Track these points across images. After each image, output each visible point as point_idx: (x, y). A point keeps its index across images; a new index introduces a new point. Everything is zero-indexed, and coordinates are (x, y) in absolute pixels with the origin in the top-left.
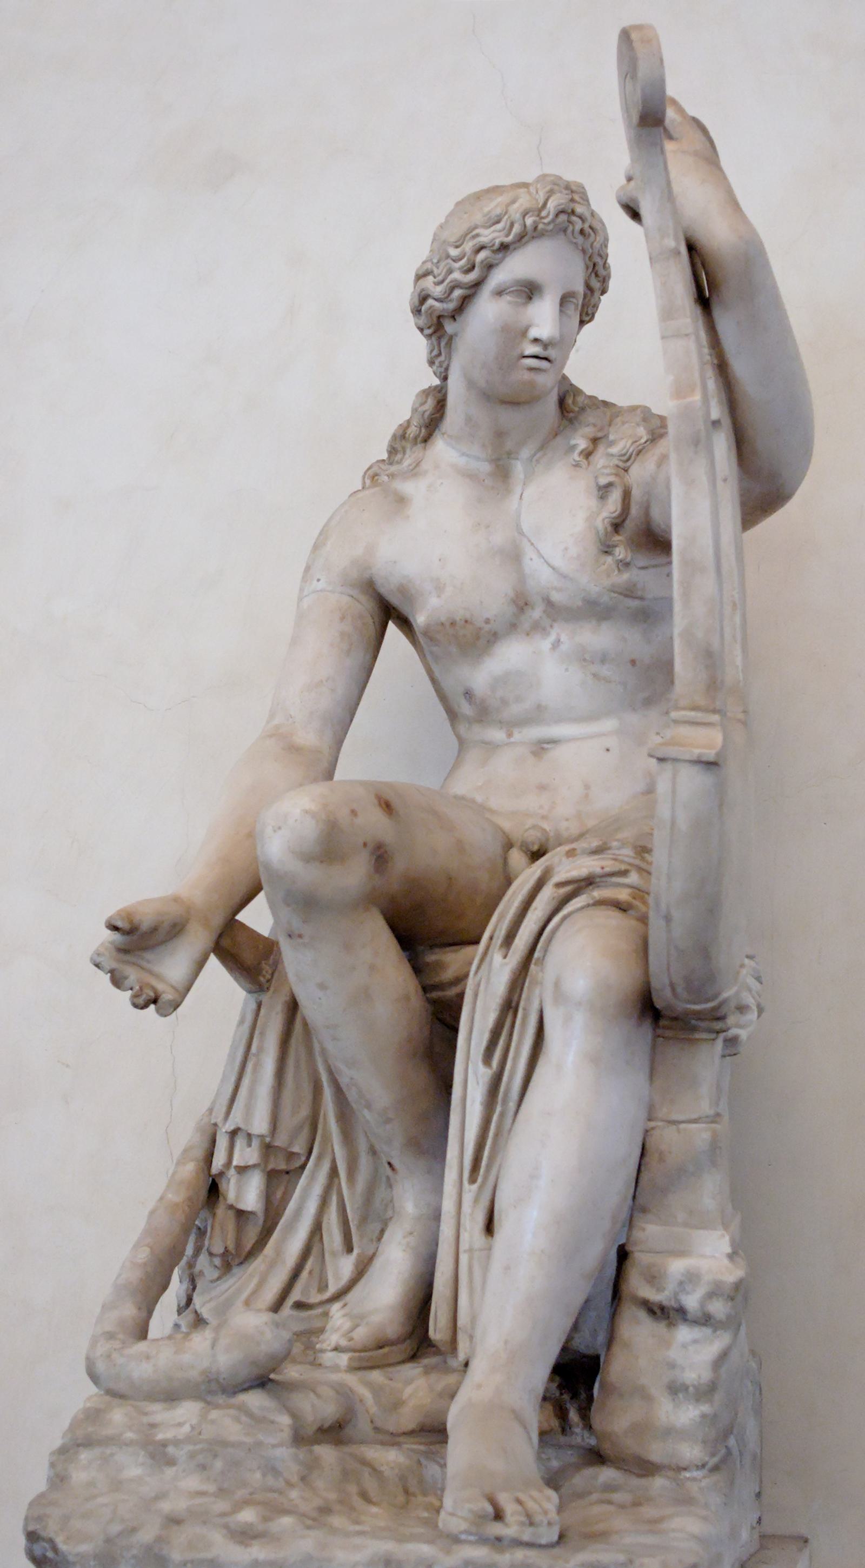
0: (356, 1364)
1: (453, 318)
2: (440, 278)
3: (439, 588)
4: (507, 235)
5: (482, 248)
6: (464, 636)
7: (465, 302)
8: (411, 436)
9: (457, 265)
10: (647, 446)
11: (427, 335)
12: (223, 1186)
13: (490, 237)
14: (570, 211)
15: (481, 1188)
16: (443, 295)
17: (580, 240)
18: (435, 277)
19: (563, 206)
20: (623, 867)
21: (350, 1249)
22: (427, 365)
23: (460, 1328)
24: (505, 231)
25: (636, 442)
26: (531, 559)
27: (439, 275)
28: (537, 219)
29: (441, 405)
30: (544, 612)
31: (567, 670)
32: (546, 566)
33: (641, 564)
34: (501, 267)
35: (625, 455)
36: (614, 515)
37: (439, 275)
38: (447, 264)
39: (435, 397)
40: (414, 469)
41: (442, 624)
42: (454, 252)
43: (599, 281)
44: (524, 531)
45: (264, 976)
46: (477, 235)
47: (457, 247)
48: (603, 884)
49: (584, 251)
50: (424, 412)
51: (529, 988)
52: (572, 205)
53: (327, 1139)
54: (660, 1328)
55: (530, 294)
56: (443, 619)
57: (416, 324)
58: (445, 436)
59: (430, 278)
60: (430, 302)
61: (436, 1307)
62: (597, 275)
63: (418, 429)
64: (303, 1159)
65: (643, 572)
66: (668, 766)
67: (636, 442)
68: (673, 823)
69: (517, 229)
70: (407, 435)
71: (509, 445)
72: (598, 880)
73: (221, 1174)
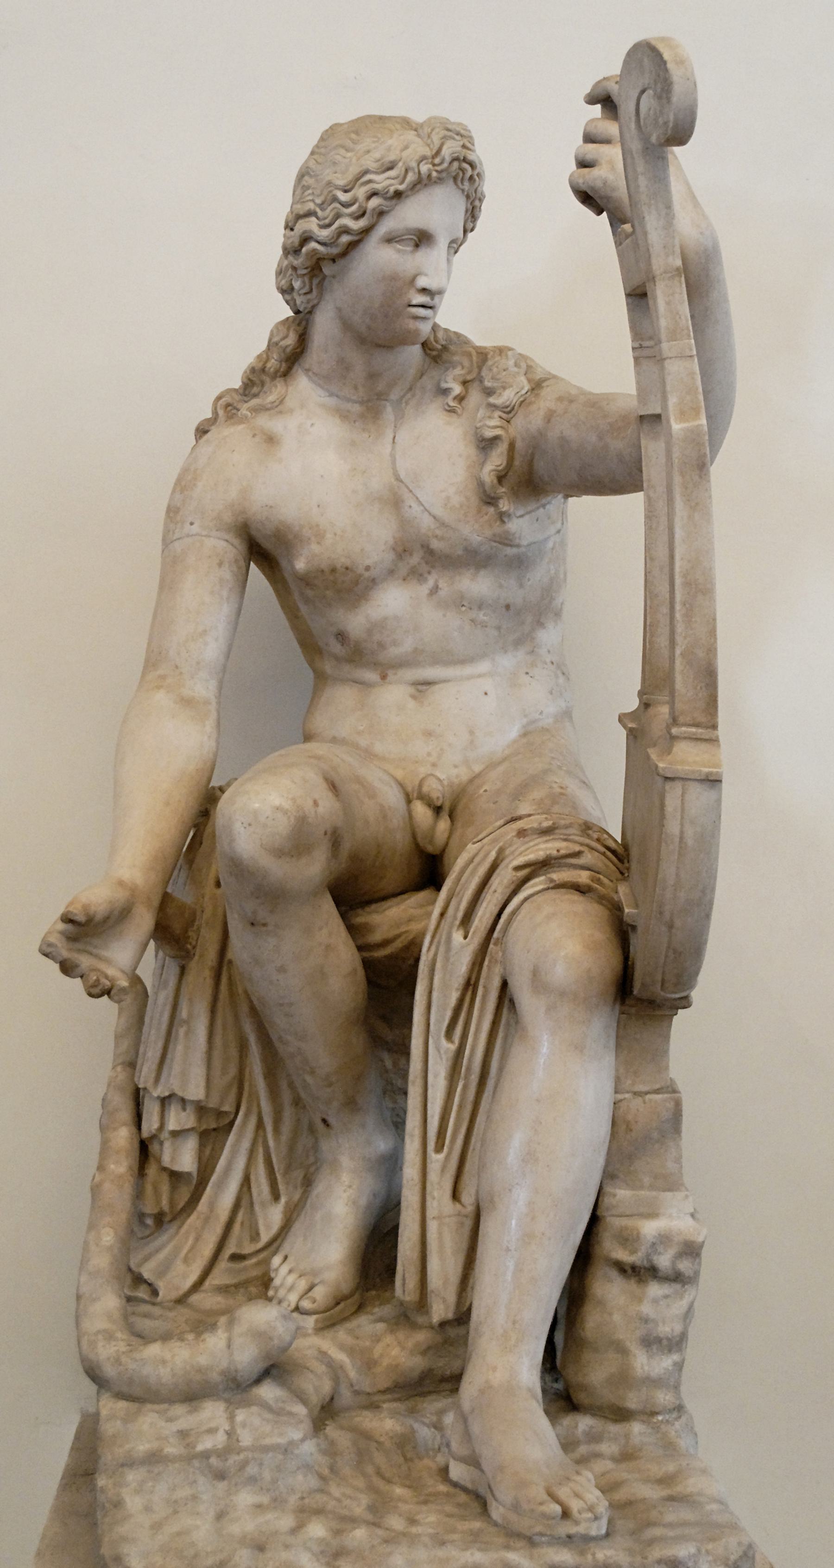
0: (320, 1325)
2: (327, 221)
3: (320, 536)
4: (402, 183)
5: (374, 194)
6: (343, 582)
7: (353, 246)
8: (272, 370)
12: (154, 1148)
14: (462, 158)
15: (447, 1158)
16: (330, 240)
17: (466, 185)
19: (456, 155)
20: (577, 848)
21: (276, 1197)
23: (432, 1291)
24: (399, 179)
25: (518, 393)
26: (410, 507)
27: (325, 218)
28: (430, 166)
29: (303, 340)
30: (423, 558)
31: (444, 616)
32: (426, 514)
33: (519, 513)
35: (507, 407)
36: (500, 468)
37: (325, 218)
38: (334, 208)
39: (297, 331)
41: (323, 571)
42: (343, 197)
44: (402, 477)
45: (191, 944)
46: (370, 181)
47: (346, 191)
48: (557, 865)
49: (468, 197)
50: (287, 347)
51: (489, 967)
53: (254, 1097)
54: (632, 1285)
56: (324, 566)
58: (310, 373)
60: (313, 245)
61: (404, 1270)
63: (279, 364)
64: (232, 1116)
65: (521, 520)
66: (678, 785)
68: (681, 838)
69: (411, 177)
70: (267, 369)
71: (381, 386)
72: (553, 862)
73: (154, 1137)
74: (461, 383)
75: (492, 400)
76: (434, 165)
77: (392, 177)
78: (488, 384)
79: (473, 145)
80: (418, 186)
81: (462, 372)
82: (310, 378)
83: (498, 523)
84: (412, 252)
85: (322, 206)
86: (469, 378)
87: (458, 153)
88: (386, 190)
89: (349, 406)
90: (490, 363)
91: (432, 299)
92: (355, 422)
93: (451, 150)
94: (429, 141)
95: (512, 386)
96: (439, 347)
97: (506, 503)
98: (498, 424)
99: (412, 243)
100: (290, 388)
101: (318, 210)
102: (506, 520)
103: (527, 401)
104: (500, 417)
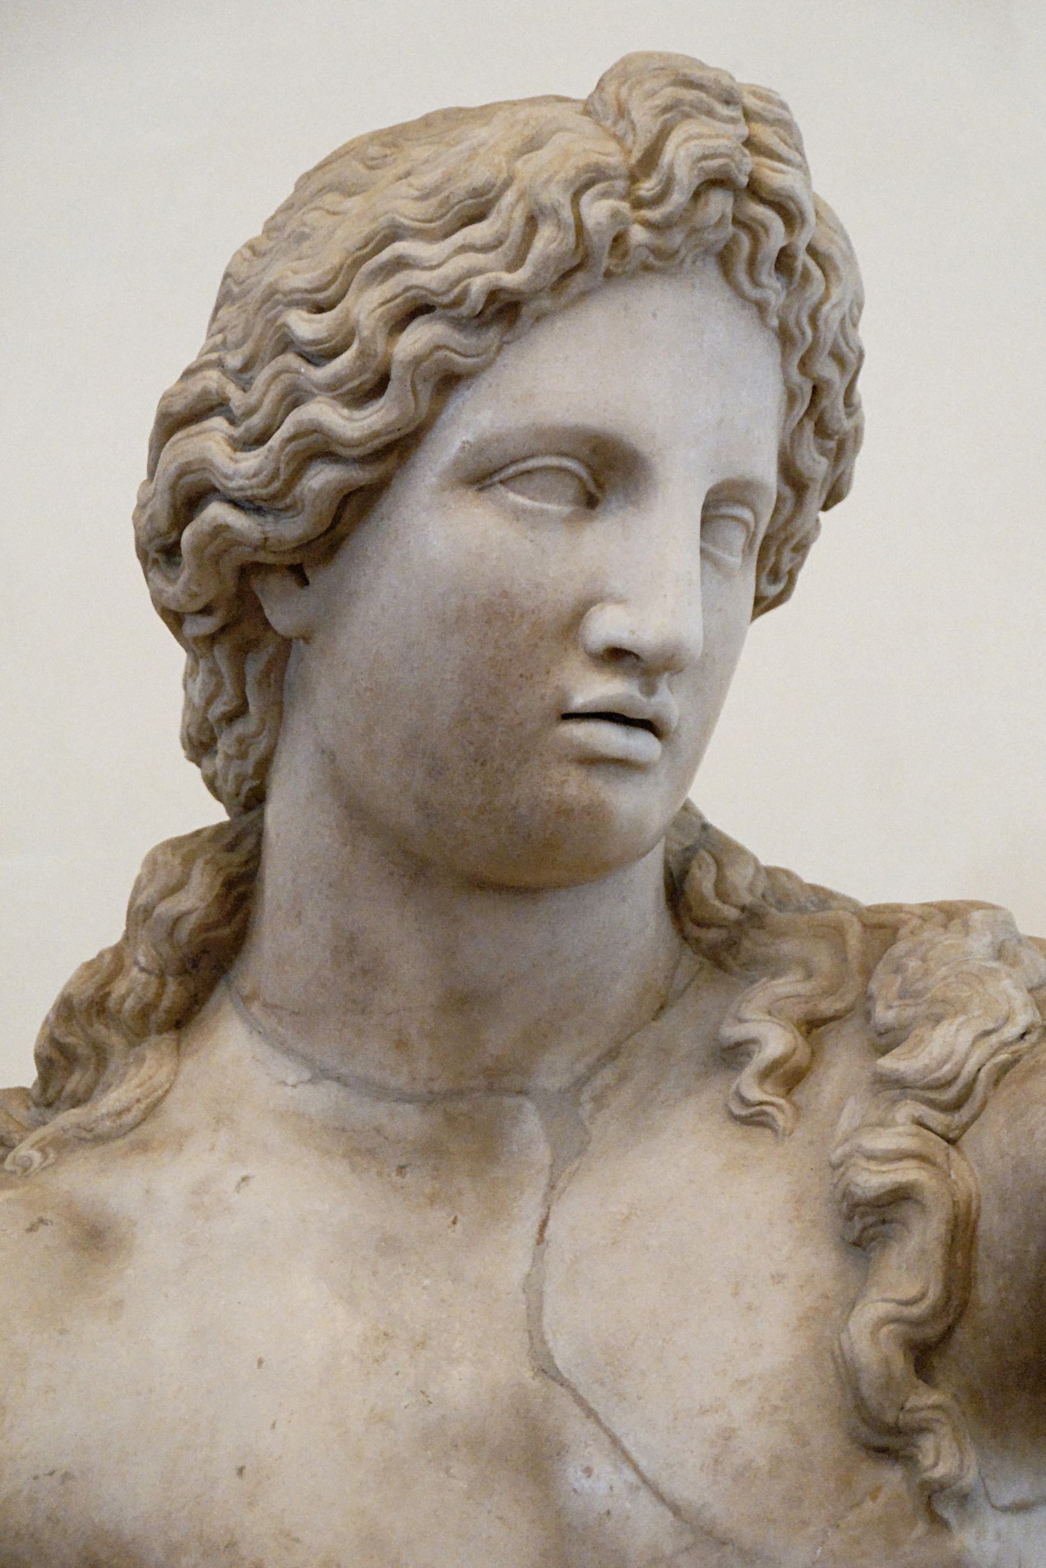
1: (299, 574)
2: (256, 421)
8: (129, 1004)
9: (323, 373)
10: (1034, 1046)
11: (196, 639)
13: (451, 269)
14: (744, 180)
18: (232, 422)
22: (179, 753)
25: (987, 1033)
27: (250, 412)
28: (625, 206)
32: (644, 1497)
34: (485, 383)
35: (949, 1083)
36: (916, 1311)
37: (250, 412)
40: (138, 1125)
43: (823, 453)
44: (558, 1363)
46: (400, 264)
47: (320, 309)
49: (785, 337)
50: (177, 920)
52: (749, 162)
55: (592, 487)
57: (156, 598)
58: (255, 1008)
59: (218, 422)
60: (216, 512)
62: (822, 430)
63: (154, 981)
67: (987, 1033)
70: (111, 1003)
74: (798, 1026)
75: (887, 1063)
76: (638, 204)
77: (479, 243)
78: (884, 1015)
79: (799, 150)
80: (579, 281)
81: (804, 988)
82: (255, 1027)
83: (921, 1528)
84: (569, 521)
85: (244, 374)
86: (827, 1007)
87: (726, 156)
88: (457, 290)
89: (379, 1113)
90: (900, 948)
91: (650, 690)
92: (401, 1169)
93: (695, 148)
94: (622, 126)
95: (964, 1009)
96: (732, 913)
97: (947, 1445)
98: (909, 1143)
99: (571, 490)
100: (189, 1065)
101: (233, 391)
102: (948, 1514)
103: (1026, 1062)
104: (920, 1123)
